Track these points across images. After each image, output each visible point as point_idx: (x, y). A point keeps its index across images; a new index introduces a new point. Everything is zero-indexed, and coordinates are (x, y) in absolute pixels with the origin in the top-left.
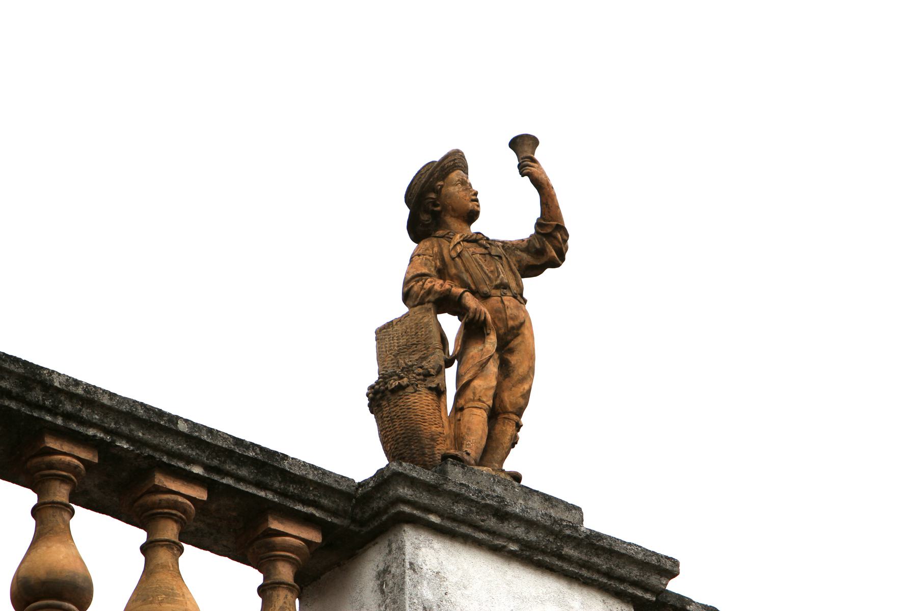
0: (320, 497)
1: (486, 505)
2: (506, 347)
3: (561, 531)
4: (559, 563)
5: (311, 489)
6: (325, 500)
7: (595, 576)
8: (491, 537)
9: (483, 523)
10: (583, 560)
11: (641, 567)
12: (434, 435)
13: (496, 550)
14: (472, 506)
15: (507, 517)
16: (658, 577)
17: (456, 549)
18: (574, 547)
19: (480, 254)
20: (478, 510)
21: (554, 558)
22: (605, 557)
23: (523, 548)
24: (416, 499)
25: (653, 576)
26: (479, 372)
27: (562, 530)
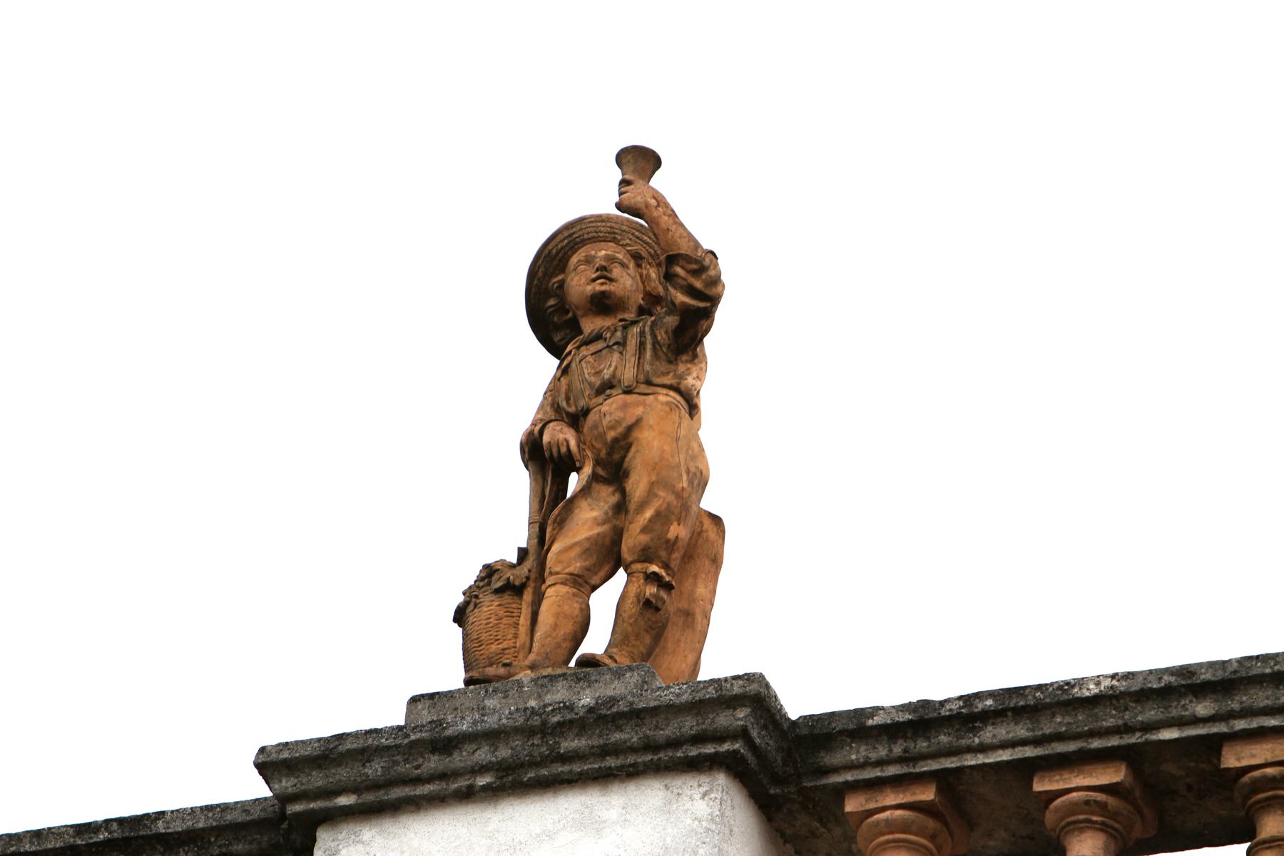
0: (230, 844)
1: (413, 744)
2: (620, 471)
3: (544, 723)
4: (566, 768)
5: (213, 839)
6: (238, 845)
7: (631, 759)
8: (444, 783)
9: (419, 771)
10: (597, 747)
11: (695, 711)
12: (492, 657)
13: (467, 796)
14: (393, 756)
15: (454, 744)
16: (731, 712)
17: (401, 825)
18: (577, 735)
19: (592, 354)
20: (406, 756)
21: (555, 764)
22: (632, 725)
23: (501, 774)
24: (303, 787)
25: (721, 715)
26: (556, 531)
27: (546, 721)
